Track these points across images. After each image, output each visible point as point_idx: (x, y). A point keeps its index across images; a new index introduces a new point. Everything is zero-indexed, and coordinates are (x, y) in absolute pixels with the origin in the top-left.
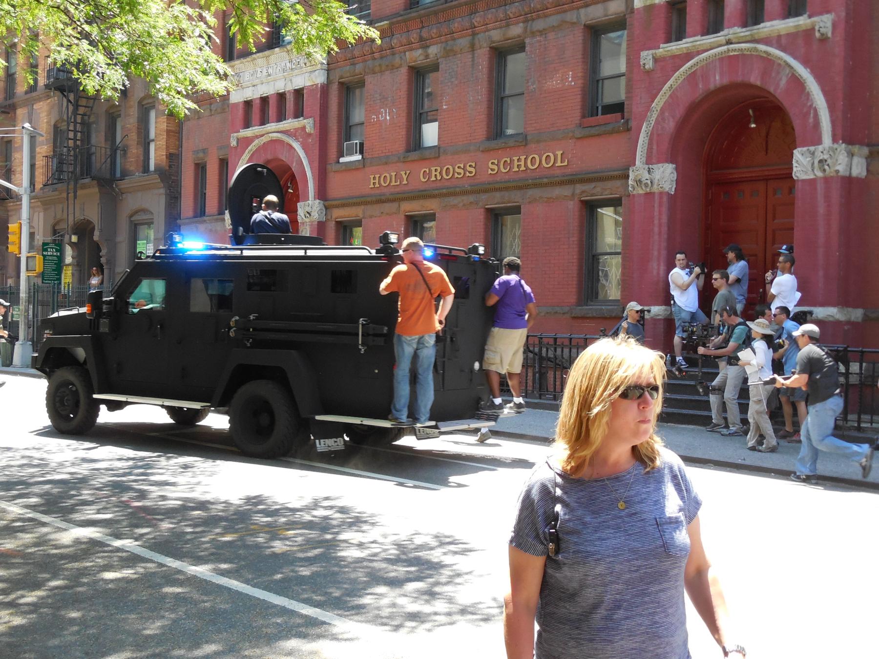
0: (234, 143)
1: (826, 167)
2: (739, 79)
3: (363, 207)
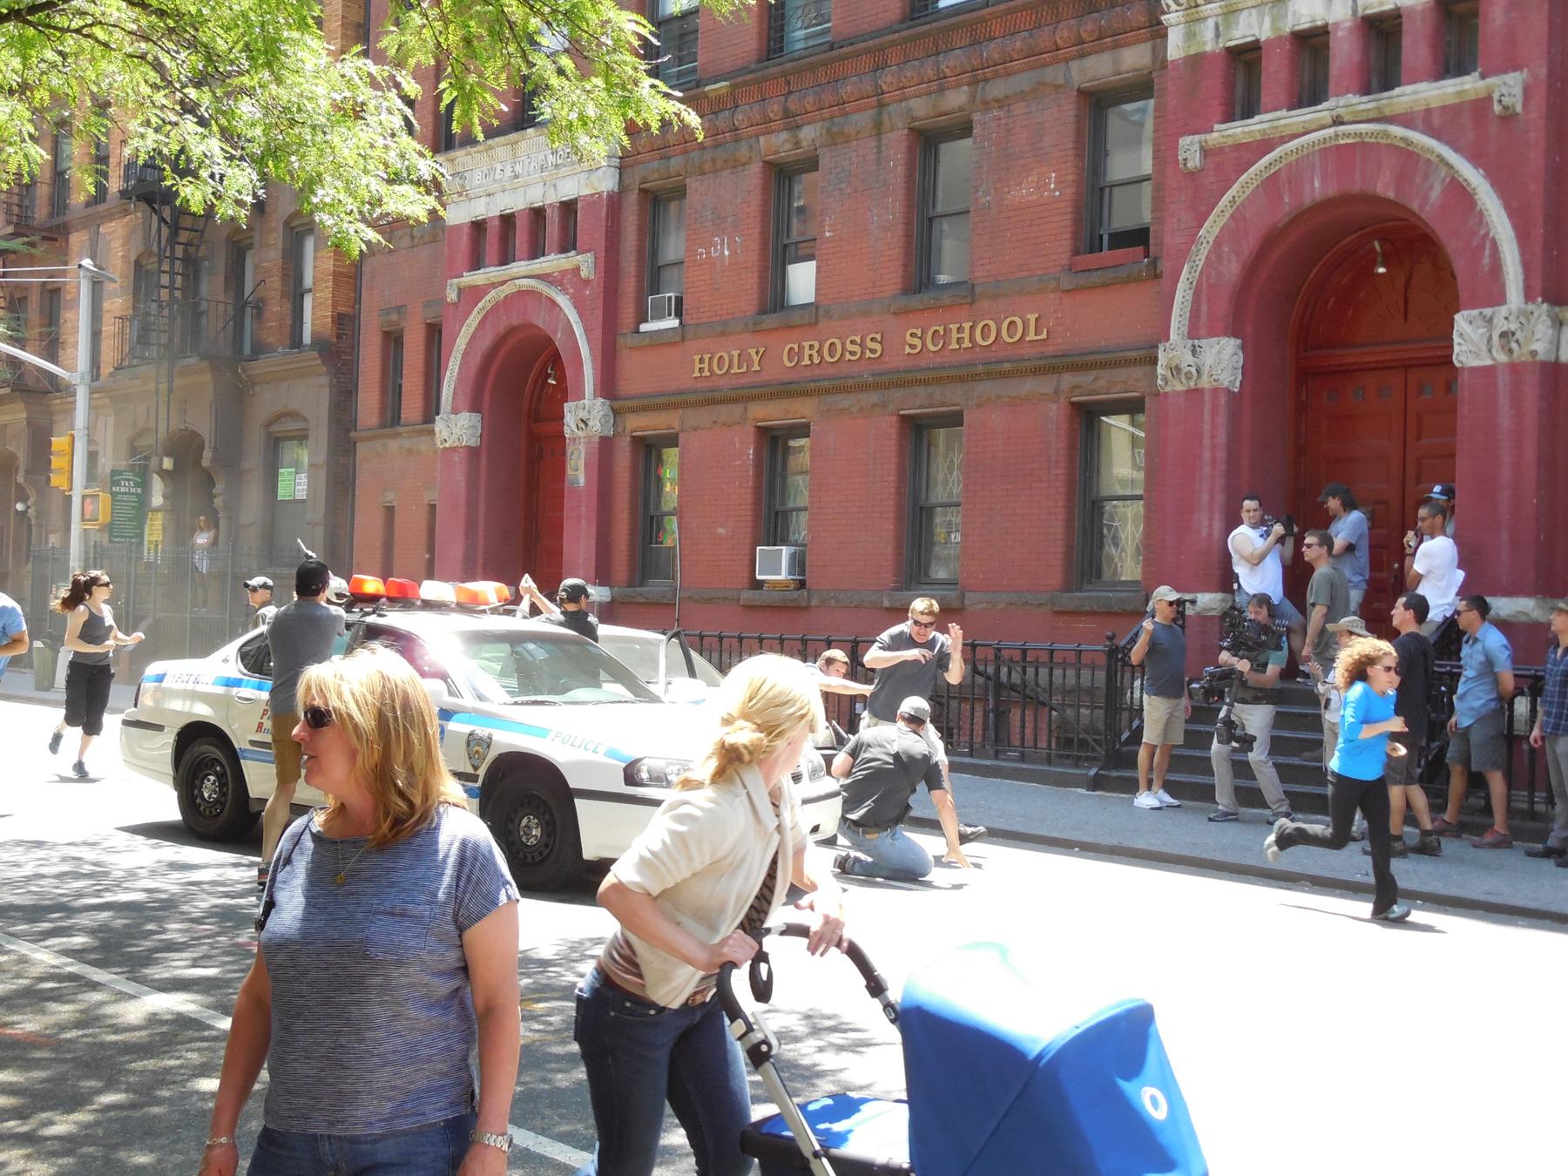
1: (1514, 345)
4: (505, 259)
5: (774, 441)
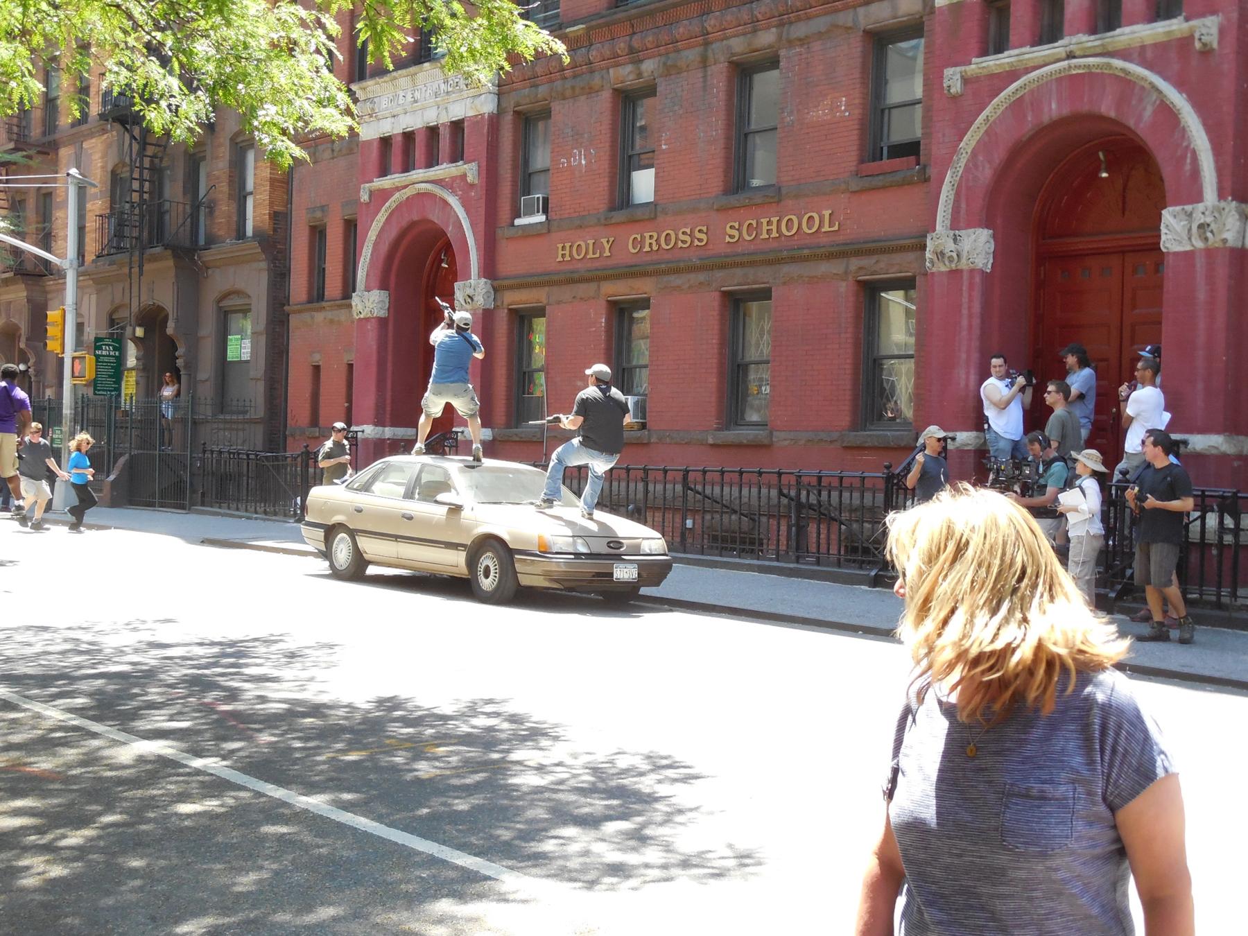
1: (1209, 235)
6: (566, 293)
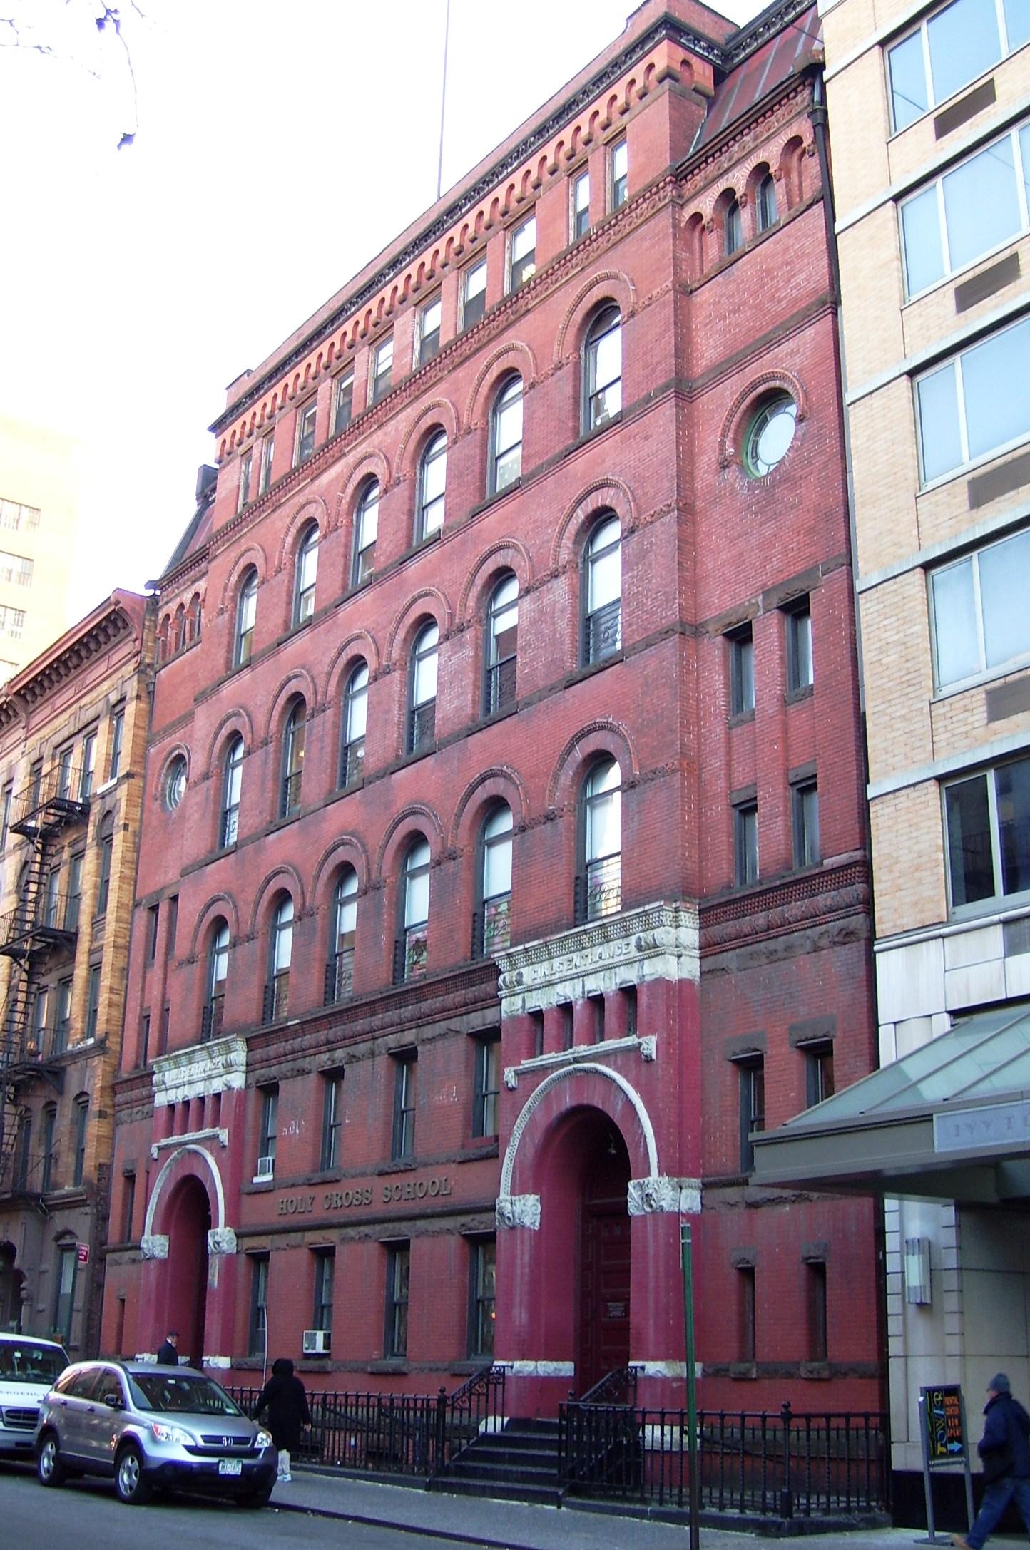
0: (155, 1152)
1: (652, 1202)
2: (585, 1102)
3: (270, 1237)
4: (184, 1132)
5: (324, 1255)
6: (280, 1240)
